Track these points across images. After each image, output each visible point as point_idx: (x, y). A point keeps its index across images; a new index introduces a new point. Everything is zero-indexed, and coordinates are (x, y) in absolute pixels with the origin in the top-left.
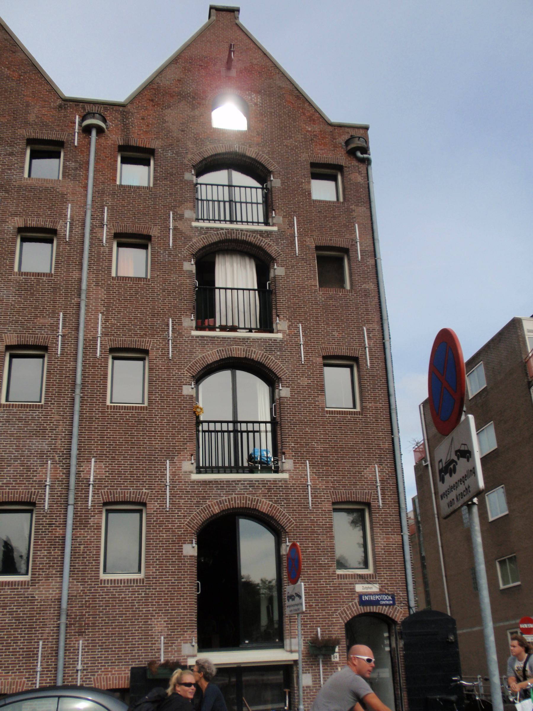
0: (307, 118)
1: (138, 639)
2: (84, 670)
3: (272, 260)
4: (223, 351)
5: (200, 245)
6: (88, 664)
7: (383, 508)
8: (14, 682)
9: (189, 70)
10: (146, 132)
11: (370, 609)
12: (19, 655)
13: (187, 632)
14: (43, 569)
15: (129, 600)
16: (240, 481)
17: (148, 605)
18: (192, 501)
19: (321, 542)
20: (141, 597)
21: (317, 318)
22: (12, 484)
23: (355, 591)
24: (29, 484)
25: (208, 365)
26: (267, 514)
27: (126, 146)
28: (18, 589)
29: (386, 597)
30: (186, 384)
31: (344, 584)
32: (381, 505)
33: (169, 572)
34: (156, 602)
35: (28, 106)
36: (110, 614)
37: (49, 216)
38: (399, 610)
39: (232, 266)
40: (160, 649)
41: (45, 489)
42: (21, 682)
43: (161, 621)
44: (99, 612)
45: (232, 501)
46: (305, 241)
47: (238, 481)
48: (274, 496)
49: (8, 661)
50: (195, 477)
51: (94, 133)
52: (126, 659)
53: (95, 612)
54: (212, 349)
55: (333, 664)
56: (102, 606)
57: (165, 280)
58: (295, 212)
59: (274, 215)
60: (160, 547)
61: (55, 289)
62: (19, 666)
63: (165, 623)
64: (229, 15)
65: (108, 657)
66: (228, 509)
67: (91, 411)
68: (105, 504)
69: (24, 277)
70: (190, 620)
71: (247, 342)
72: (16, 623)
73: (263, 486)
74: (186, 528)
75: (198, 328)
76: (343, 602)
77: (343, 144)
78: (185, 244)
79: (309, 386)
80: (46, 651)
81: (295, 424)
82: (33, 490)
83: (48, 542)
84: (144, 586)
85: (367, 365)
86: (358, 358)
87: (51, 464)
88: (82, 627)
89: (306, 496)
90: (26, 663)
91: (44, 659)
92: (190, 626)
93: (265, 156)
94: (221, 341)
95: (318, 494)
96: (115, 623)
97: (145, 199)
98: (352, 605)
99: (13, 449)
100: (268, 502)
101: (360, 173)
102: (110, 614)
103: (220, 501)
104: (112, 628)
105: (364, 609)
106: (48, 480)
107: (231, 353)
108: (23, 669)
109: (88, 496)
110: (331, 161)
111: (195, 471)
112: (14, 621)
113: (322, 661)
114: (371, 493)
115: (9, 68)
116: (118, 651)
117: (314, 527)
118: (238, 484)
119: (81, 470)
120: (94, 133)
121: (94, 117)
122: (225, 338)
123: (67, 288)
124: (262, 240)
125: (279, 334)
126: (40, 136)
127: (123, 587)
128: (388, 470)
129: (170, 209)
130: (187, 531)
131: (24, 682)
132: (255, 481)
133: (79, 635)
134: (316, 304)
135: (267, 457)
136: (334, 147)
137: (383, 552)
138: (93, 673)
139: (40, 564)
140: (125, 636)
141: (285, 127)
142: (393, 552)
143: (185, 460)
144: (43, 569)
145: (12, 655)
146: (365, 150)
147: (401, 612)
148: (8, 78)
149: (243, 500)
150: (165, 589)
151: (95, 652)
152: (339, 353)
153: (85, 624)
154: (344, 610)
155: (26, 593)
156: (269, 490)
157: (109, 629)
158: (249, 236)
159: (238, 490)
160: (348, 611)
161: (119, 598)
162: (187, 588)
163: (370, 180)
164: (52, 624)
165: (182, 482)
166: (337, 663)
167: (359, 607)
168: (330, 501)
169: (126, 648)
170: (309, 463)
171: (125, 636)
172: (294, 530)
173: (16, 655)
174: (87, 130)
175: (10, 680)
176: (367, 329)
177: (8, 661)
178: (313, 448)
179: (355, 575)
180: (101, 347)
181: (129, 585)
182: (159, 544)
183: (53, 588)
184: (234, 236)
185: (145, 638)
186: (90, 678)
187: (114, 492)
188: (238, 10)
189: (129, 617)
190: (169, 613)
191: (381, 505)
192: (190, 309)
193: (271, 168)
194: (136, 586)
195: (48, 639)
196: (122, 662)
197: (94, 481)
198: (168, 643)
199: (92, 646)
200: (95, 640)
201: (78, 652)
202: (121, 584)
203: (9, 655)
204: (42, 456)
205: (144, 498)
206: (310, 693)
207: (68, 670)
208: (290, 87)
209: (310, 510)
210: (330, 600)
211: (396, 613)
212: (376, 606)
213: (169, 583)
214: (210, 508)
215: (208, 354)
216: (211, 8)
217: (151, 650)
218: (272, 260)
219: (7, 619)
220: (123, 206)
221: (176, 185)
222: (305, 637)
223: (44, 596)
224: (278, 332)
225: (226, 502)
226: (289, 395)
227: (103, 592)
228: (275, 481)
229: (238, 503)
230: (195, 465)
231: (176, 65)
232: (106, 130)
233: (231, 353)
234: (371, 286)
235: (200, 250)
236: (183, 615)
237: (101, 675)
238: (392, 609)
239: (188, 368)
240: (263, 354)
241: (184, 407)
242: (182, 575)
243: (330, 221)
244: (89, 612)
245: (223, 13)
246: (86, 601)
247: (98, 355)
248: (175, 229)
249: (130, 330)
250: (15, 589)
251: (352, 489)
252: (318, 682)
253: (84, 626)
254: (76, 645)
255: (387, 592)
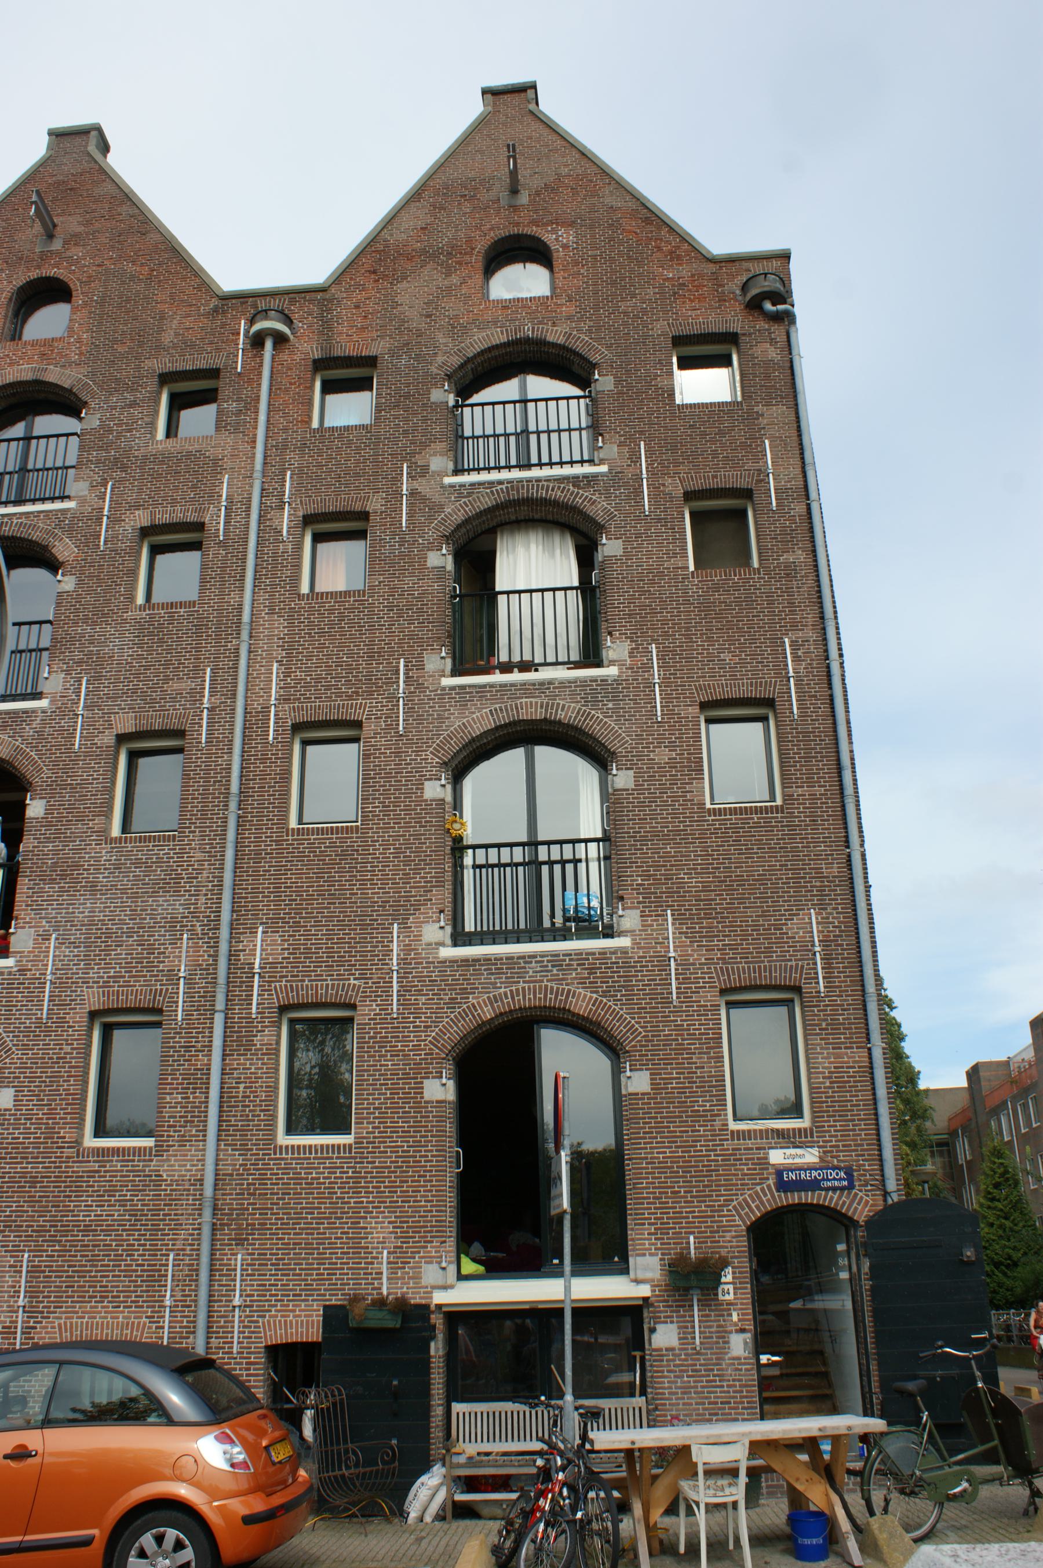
0: (666, 256)
1: (342, 1253)
2: (246, 1306)
3: (600, 528)
4: (501, 710)
5: (460, 517)
6: (253, 1295)
7: (826, 996)
8: (128, 1323)
9: (442, 208)
10: (363, 329)
11: (800, 1198)
12: (136, 1276)
13: (432, 1242)
14: (175, 1126)
15: (324, 1183)
16: (535, 957)
17: (361, 1192)
18: (441, 999)
19: (696, 1068)
20: (347, 1178)
21: (688, 629)
22: (124, 977)
23: (768, 1163)
24: (151, 976)
25: (473, 740)
26: (587, 1018)
27: (326, 358)
28: (133, 1161)
29: (834, 1174)
30: (431, 779)
31: (745, 1149)
32: (822, 989)
33: (398, 1132)
34: (373, 1187)
35: (162, 318)
36: (292, 1208)
37: (192, 500)
38: (862, 1198)
39: (528, 548)
40: (381, 1273)
41: (178, 984)
42: (139, 1323)
43: (384, 1222)
44: (272, 1204)
45: (518, 995)
46: (664, 485)
47: (529, 957)
48: (602, 982)
49: (118, 1286)
50: (449, 952)
51: (269, 344)
52: (320, 1290)
53: (264, 1204)
54: (480, 710)
55: (722, 1305)
56: (278, 1194)
57: (393, 589)
58: (641, 433)
59: (600, 444)
60: (381, 1085)
61: (200, 627)
62: (136, 1296)
63: (391, 1226)
64: (516, 99)
65: (288, 1285)
66: (511, 1011)
67: (258, 841)
68: (283, 1009)
69: (148, 612)
70: (436, 1221)
71: (549, 688)
72: (130, 1220)
73: (578, 965)
74: (430, 1049)
75: (456, 672)
76: (742, 1185)
77: (738, 292)
78: (430, 518)
79: (672, 764)
80: (181, 1271)
81: (644, 840)
82: (159, 987)
83: (183, 1079)
84: (351, 1158)
85: (793, 713)
86: (773, 699)
87: (188, 939)
88: (243, 1229)
89: (667, 979)
90: (148, 1291)
91: (178, 1285)
92: (437, 1231)
93: (582, 336)
94: (497, 691)
95: (691, 974)
96: (300, 1223)
97: (358, 448)
98: (762, 1189)
99: (125, 915)
100: (589, 994)
101: (773, 342)
102: (292, 1208)
103: (494, 996)
104: (295, 1234)
105: (787, 1198)
106: (183, 968)
107: (518, 712)
108: (143, 1301)
109: (252, 995)
110: (713, 329)
111: (448, 941)
112: (127, 1217)
113: (699, 1300)
114: (802, 967)
115: (134, 263)
116: (306, 1275)
117: (683, 1040)
118: (531, 962)
119: (241, 948)
120: (269, 344)
121: (266, 318)
122: (505, 685)
123: (219, 623)
124: (578, 493)
125: (611, 667)
126: (180, 366)
127: (314, 1158)
128: (837, 918)
129: (404, 459)
130: (432, 1054)
131: (145, 1323)
132: (564, 955)
133: (237, 1245)
134: (687, 602)
135: (589, 908)
136: (719, 301)
137: (828, 1084)
138: (262, 1312)
139: (169, 1117)
140: (318, 1249)
141: (623, 279)
142: (850, 1082)
143: (428, 922)
144: (175, 1126)
145: (125, 1276)
146: (782, 296)
147: (867, 1202)
148: (132, 278)
149: (540, 993)
150: (391, 1162)
151: (266, 1275)
152: (735, 694)
153: (248, 1225)
154: (745, 1200)
155: (147, 1169)
156: (592, 970)
157: (289, 1234)
158: (553, 490)
159: (531, 974)
160: (753, 1201)
161: (307, 1178)
162: (432, 1161)
163: (794, 352)
164: (191, 1224)
165: (422, 963)
166: (730, 1304)
167: (776, 1194)
168: (716, 987)
169: (319, 1269)
170: (673, 915)
171: (318, 1249)
172: (641, 1046)
173: (131, 1276)
174: (257, 341)
175: (121, 1319)
176: (792, 642)
177: (118, 1286)
178: (681, 885)
179: (767, 1130)
180: (275, 723)
181: (325, 1155)
182: (379, 1080)
183: (192, 1160)
184: (523, 493)
185: (353, 1253)
186: (257, 1322)
187: (297, 986)
188: (533, 86)
189: (325, 1213)
190: (398, 1207)
191: (822, 989)
192: (439, 638)
193: (595, 358)
194: (337, 1158)
195: (184, 1250)
196: (313, 1295)
197: (261, 968)
198: (397, 1263)
199: (259, 1265)
200: (266, 1254)
201: (235, 1275)
202: (310, 1153)
203: (120, 1276)
204: (174, 925)
205: (351, 996)
206: (674, 1360)
207: (219, 1306)
208: (632, 205)
209: (675, 1007)
210: (716, 1180)
211: (855, 1205)
212: (813, 1191)
213: (398, 1152)
214: (476, 1010)
215: (473, 719)
216: (485, 92)
217: (365, 1274)
218: (600, 528)
219: (116, 1214)
220: (320, 466)
221: (415, 413)
222: (662, 1254)
223: (177, 1174)
224: (612, 663)
225: (507, 998)
226: (631, 785)
227: (278, 1169)
228: (603, 953)
229: (530, 999)
230: (449, 929)
231: (418, 204)
232: (291, 337)
233: (518, 712)
234: (799, 556)
235: (459, 527)
236: (424, 1211)
237: (277, 1316)
238: (847, 1198)
239: (435, 749)
240: (580, 709)
241: (426, 822)
242: (421, 1136)
243: (713, 441)
244: (255, 1204)
245: (507, 98)
246: (248, 1184)
247: (271, 738)
248: (413, 493)
249: (328, 688)
250: (128, 1161)
251: (763, 962)
252: (690, 1341)
253: (246, 1229)
254: (233, 1262)
255: (835, 1162)
